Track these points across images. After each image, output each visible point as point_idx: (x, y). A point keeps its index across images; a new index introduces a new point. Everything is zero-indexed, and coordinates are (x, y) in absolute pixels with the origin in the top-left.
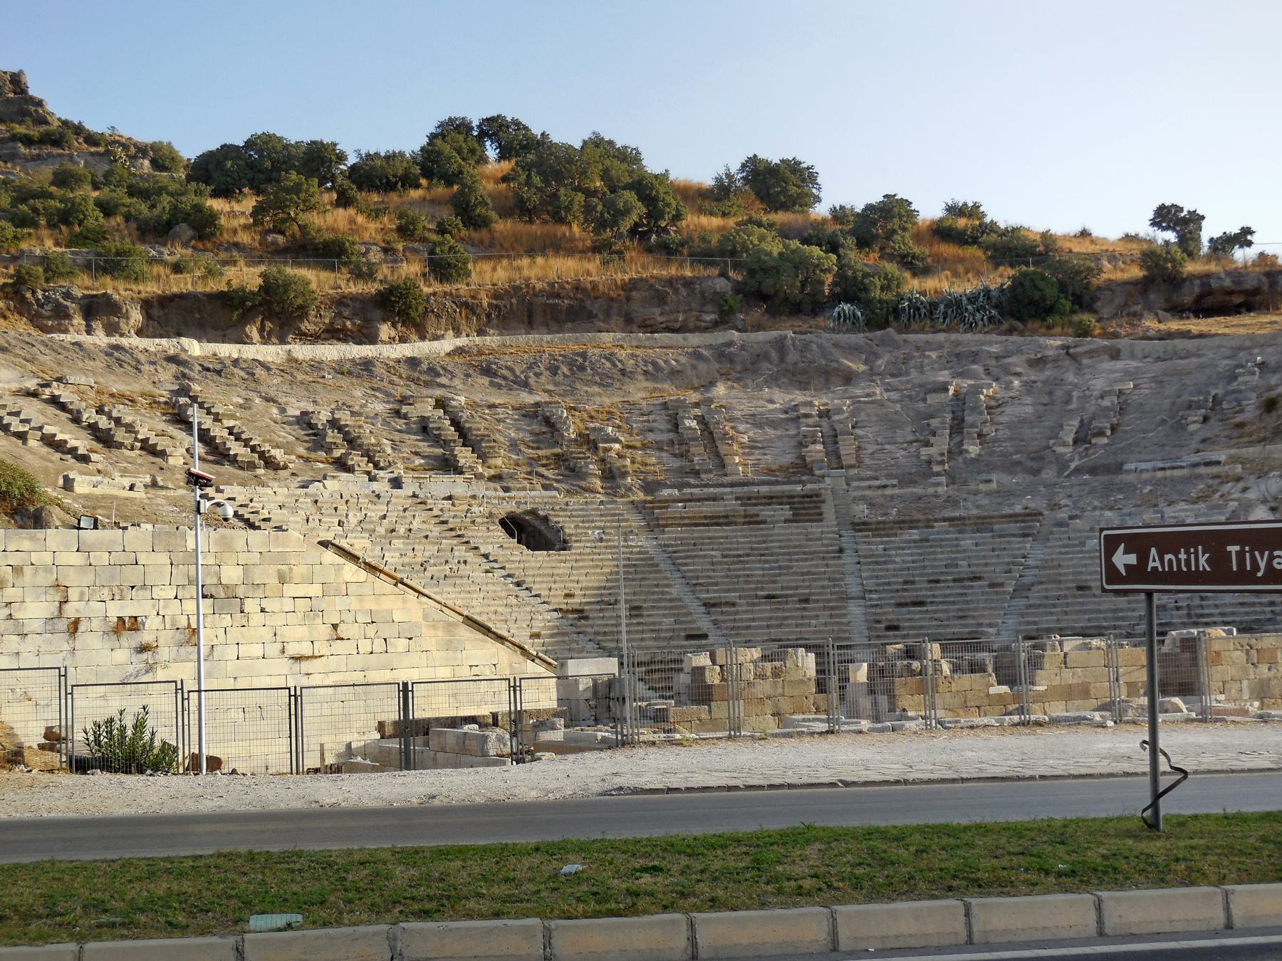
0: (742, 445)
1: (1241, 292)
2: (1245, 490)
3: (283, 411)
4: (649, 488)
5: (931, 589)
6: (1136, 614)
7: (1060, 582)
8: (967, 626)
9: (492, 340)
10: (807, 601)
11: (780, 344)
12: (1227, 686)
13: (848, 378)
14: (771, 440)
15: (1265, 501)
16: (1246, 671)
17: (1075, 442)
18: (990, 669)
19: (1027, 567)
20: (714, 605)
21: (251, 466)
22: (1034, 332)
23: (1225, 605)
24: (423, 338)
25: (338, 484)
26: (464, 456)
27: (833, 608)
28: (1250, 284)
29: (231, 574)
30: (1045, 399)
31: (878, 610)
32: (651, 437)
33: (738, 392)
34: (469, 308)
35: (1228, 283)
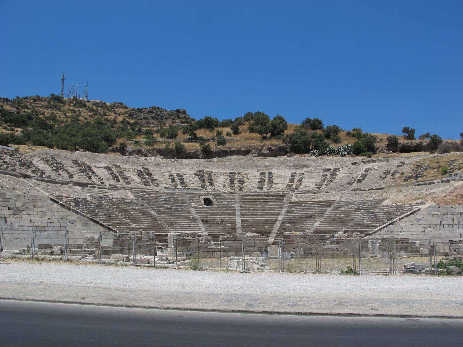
29: (19, 204)
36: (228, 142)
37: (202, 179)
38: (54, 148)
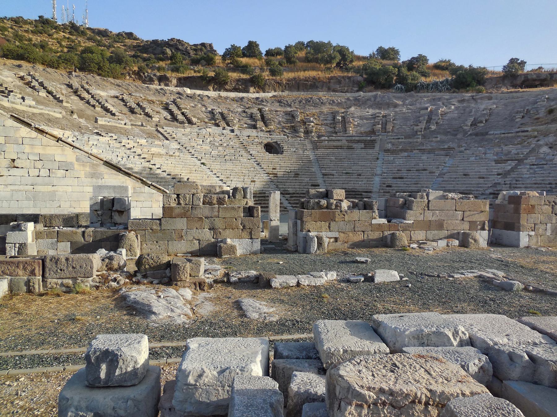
0: (354, 125)
1: (539, 80)
2: (538, 140)
3: (206, 109)
4: (319, 137)
5: (407, 173)
6: (487, 186)
7: (457, 172)
8: (417, 187)
9: (286, 93)
10: (360, 175)
11: (375, 97)
12: (537, 226)
13: (396, 106)
14: (365, 124)
15: (547, 145)
16: (550, 219)
17: (471, 125)
18: (375, 208)
19: (445, 167)
20: (326, 175)
21: (182, 123)
22: (462, 92)
23: (527, 184)
24: (264, 92)
25: (213, 130)
26: (260, 124)
27: (369, 178)
28: (543, 77)
30: (462, 112)
31: (385, 180)
32: (325, 122)
33: (358, 109)
34: (279, 84)
35: (534, 77)
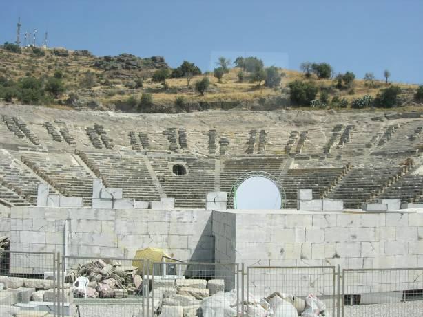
36: (404, 101)
37: (172, 140)
38: (14, 100)
